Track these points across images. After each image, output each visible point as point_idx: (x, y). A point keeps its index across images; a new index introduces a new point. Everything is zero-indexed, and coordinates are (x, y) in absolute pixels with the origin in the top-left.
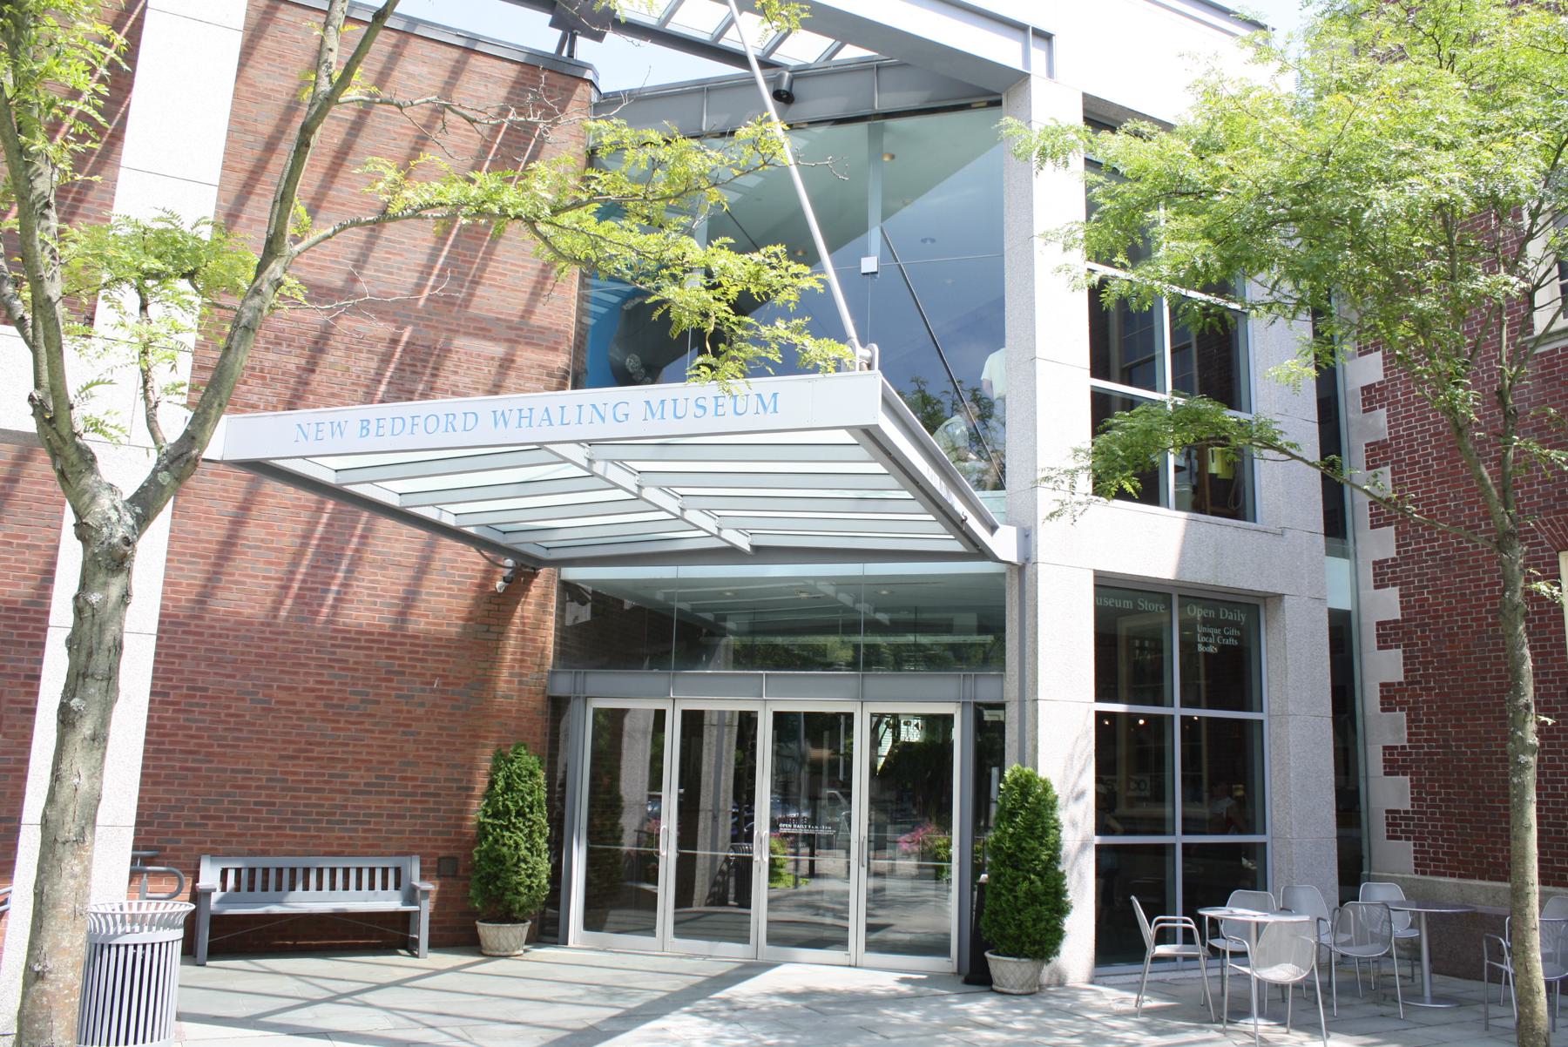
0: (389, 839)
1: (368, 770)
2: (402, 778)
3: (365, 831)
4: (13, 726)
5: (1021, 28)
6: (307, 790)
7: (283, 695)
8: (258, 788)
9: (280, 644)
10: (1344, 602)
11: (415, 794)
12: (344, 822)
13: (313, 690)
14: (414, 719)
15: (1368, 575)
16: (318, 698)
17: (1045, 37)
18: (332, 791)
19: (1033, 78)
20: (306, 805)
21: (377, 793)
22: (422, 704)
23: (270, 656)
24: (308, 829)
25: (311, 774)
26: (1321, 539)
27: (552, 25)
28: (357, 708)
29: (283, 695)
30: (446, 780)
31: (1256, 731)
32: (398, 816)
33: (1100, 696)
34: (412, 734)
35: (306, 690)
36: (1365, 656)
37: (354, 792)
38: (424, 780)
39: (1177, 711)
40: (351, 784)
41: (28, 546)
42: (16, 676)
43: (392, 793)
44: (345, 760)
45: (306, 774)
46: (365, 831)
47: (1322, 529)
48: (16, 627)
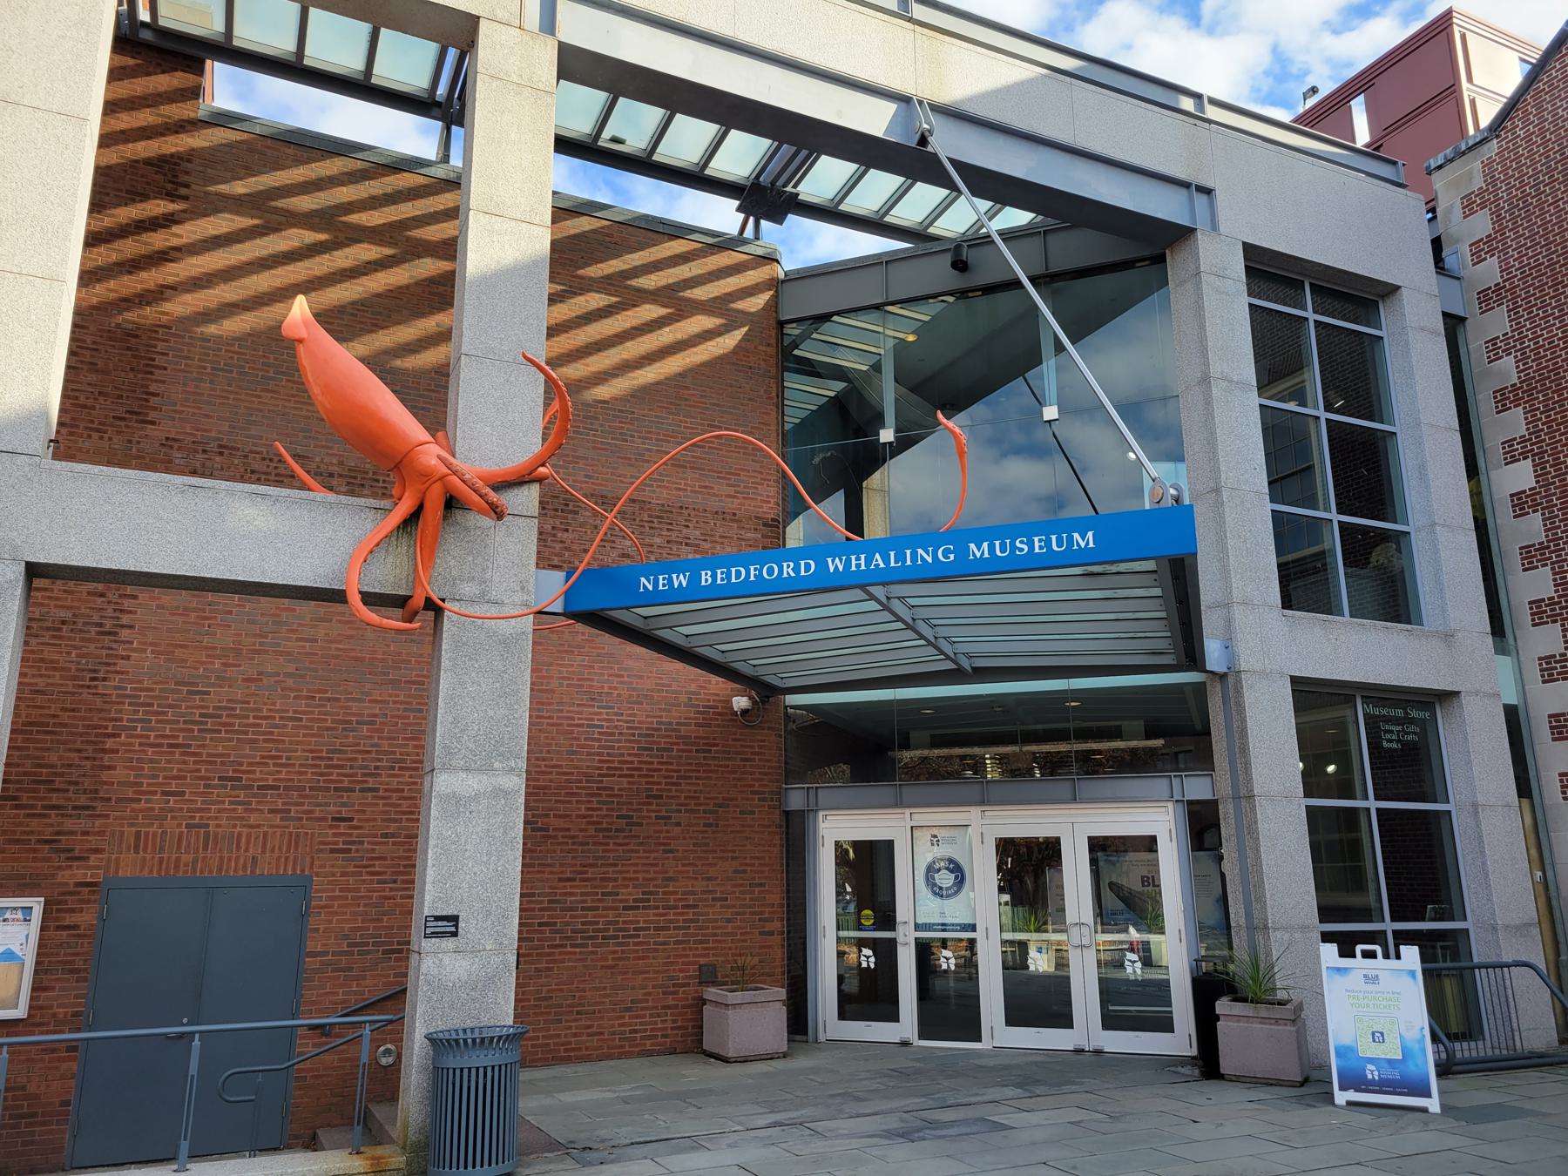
0: (656, 950)
1: (635, 887)
2: (664, 893)
3: (635, 944)
4: (323, 866)
5: (1186, 185)
6: (583, 909)
7: (561, 823)
8: (541, 910)
9: (553, 776)
10: (1513, 700)
11: (676, 907)
12: (617, 937)
13: (584, 817)
14: (673, 838)
15: (1533, 672)
16: (589, 823)
17: (1208, 192)
18: (605, 909)
19: (1199, 233)
20: (583, 924)
21: (644, 908)
22: (678, 824)
23: (545, 788)
24: (586, 945)
25: (587, 894)
26: (1490, 638)
27: (739, 209)
28: (622, 830)
29: (561, 823)
30: (703, 892)
31: (1444, 824)
32: (662, 929)
33: (1307, 794)
34: (671, 851)
35: (578, 816)
36: (1537, 747)
37: (625, 908)
38: (684, 893)
39: (1373, 804)
40: (621, 901)
41: (329, 699)
42: (323, 819)
43: (657, 908)
44: (616, 880)
45: (583, 894)
46: (635, 944)
47: (1488, 629)
48: (321, 774)
